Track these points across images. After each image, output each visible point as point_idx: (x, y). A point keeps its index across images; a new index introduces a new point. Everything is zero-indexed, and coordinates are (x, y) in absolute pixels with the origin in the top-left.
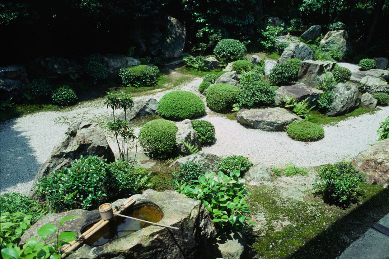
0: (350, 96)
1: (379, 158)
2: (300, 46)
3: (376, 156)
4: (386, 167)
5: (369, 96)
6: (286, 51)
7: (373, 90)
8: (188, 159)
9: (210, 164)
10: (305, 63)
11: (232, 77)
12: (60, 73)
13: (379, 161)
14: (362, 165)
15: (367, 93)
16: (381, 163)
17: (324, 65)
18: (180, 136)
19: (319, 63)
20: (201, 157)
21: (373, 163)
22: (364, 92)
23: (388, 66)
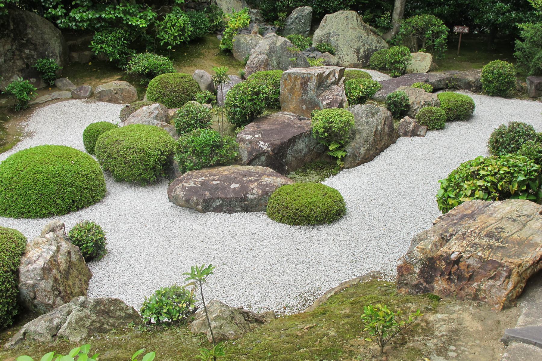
0: (379, 128)
1: (453, 250)
2: (279, 44)
3: (445, 249)
4: (468, 267)
5: (410, 123)
6: (254, 55)
7: (416, 110)
8: (51, 321)
9: (105, 321)
10: (289, 74)
11: (153, 116)
12: (26, 51)
13: (453, 257)
14: (422, 272)
15: (407, 118)
16: (457, 261)
17: (325, 74)
18: (30, 267)
19: (315, 71)
20: (80, 311)
21: (443, 263)
22: (403, 114)
23: (265, 336)
